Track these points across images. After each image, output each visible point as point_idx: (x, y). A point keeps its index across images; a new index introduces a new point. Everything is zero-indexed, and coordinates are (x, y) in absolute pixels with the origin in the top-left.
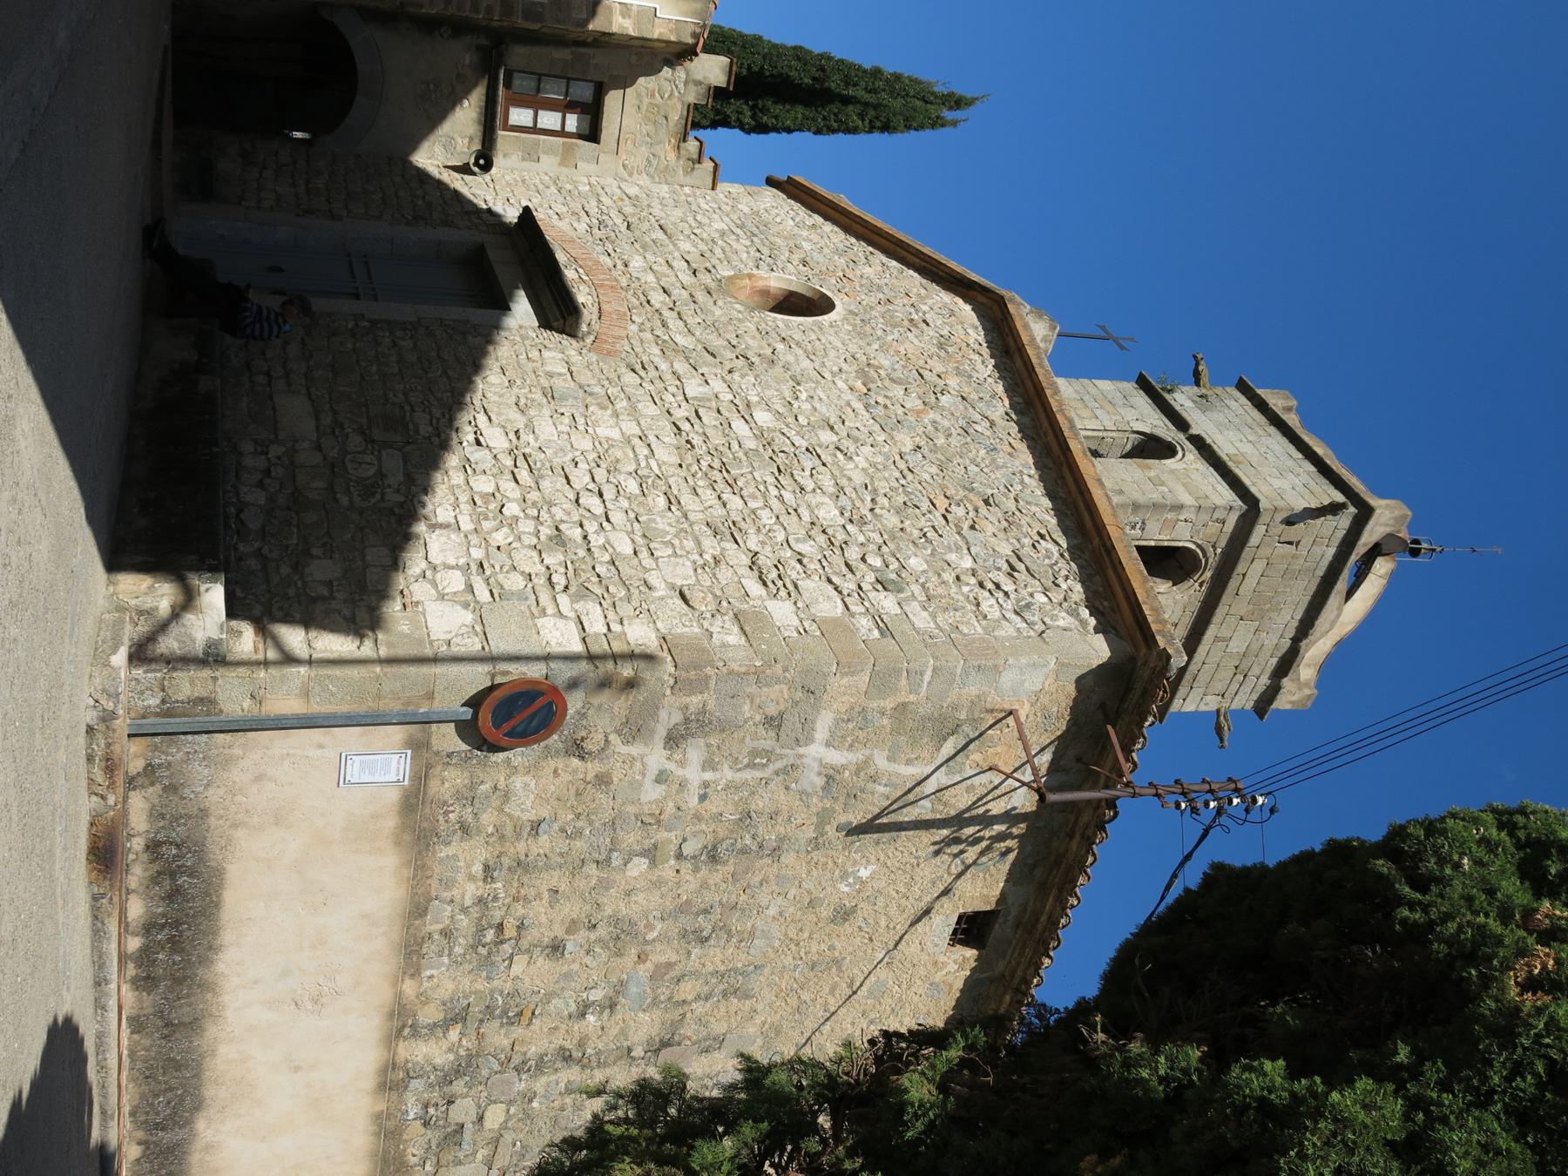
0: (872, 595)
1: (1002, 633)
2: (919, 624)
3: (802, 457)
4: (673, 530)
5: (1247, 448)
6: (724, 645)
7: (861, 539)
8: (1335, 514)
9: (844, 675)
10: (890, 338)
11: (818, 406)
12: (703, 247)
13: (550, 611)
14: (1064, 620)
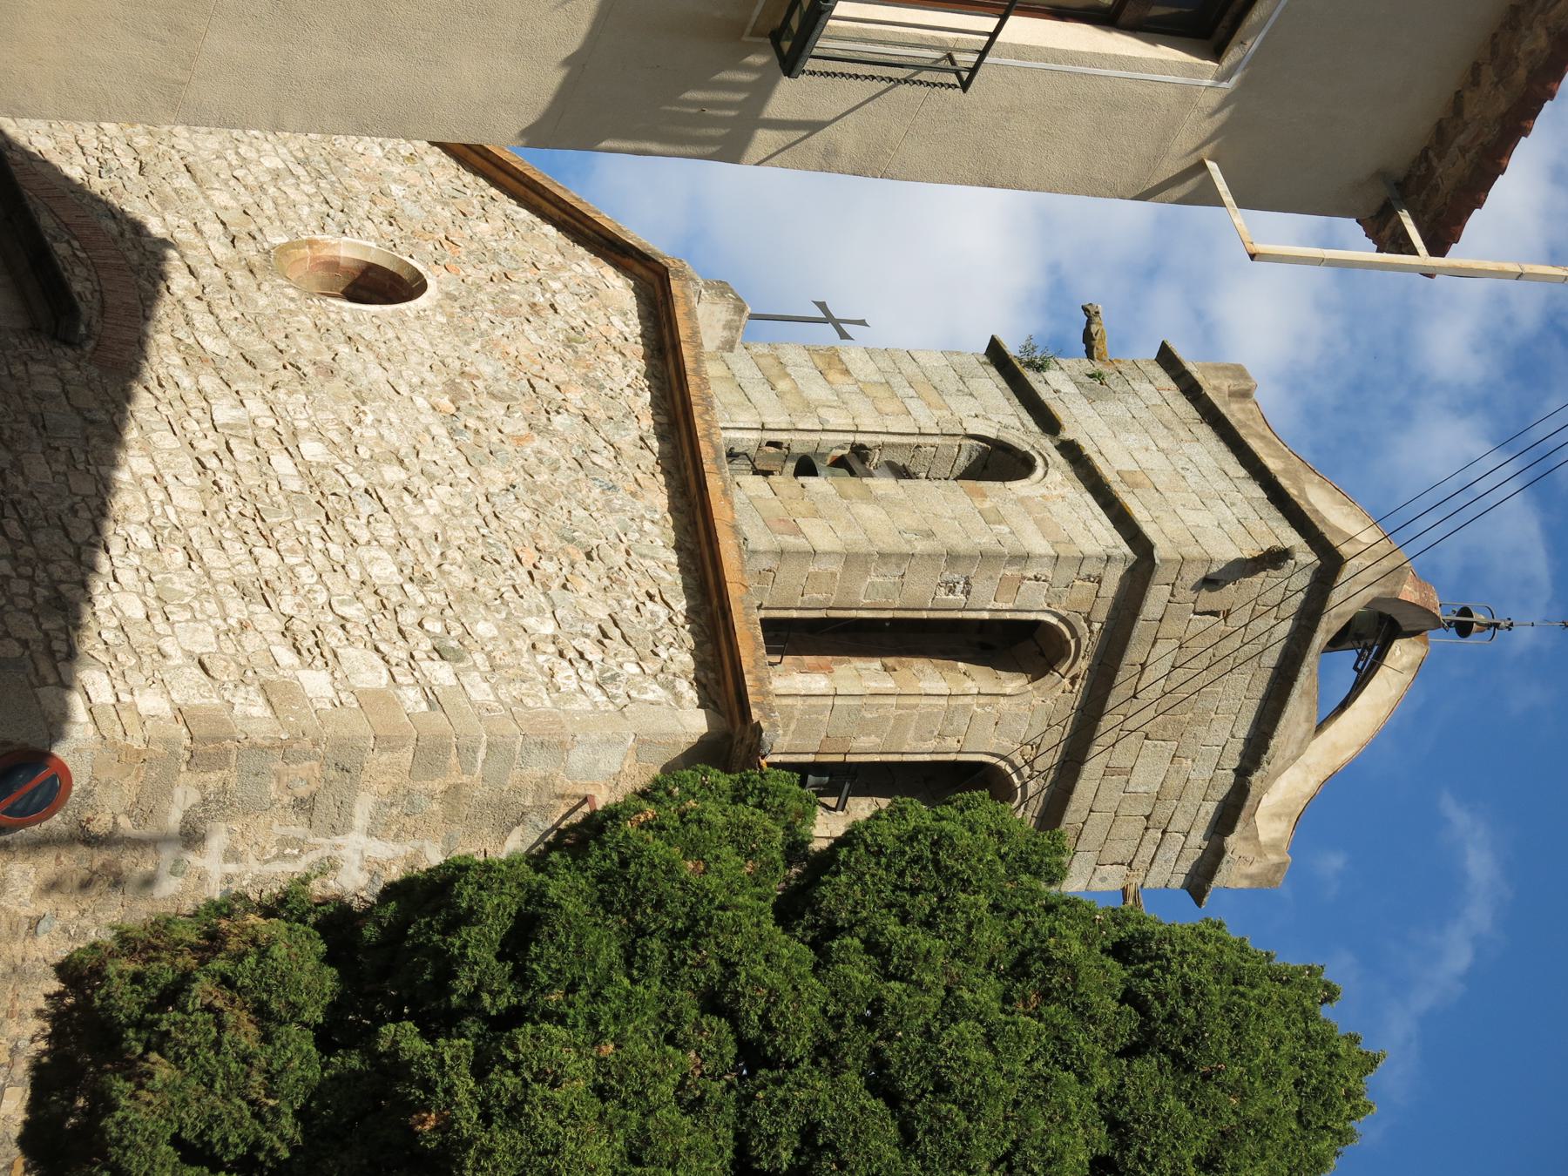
0: (425, 665)
1: (575, 707)
2: (476, 696)
3: (358, 501)
4: (192, 591)
5: (1153, 461)
6: (247, 717)
7: (421, 600)
8: (1277, 568)
9: (382, 750)
10: (499, 332)
11: (385, 432)
12: (247, 199)
13: (51, 681)
14: (655, 692)
